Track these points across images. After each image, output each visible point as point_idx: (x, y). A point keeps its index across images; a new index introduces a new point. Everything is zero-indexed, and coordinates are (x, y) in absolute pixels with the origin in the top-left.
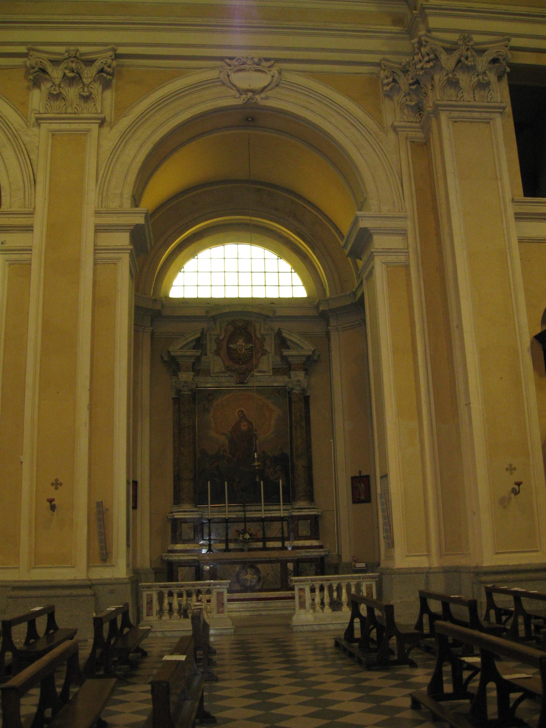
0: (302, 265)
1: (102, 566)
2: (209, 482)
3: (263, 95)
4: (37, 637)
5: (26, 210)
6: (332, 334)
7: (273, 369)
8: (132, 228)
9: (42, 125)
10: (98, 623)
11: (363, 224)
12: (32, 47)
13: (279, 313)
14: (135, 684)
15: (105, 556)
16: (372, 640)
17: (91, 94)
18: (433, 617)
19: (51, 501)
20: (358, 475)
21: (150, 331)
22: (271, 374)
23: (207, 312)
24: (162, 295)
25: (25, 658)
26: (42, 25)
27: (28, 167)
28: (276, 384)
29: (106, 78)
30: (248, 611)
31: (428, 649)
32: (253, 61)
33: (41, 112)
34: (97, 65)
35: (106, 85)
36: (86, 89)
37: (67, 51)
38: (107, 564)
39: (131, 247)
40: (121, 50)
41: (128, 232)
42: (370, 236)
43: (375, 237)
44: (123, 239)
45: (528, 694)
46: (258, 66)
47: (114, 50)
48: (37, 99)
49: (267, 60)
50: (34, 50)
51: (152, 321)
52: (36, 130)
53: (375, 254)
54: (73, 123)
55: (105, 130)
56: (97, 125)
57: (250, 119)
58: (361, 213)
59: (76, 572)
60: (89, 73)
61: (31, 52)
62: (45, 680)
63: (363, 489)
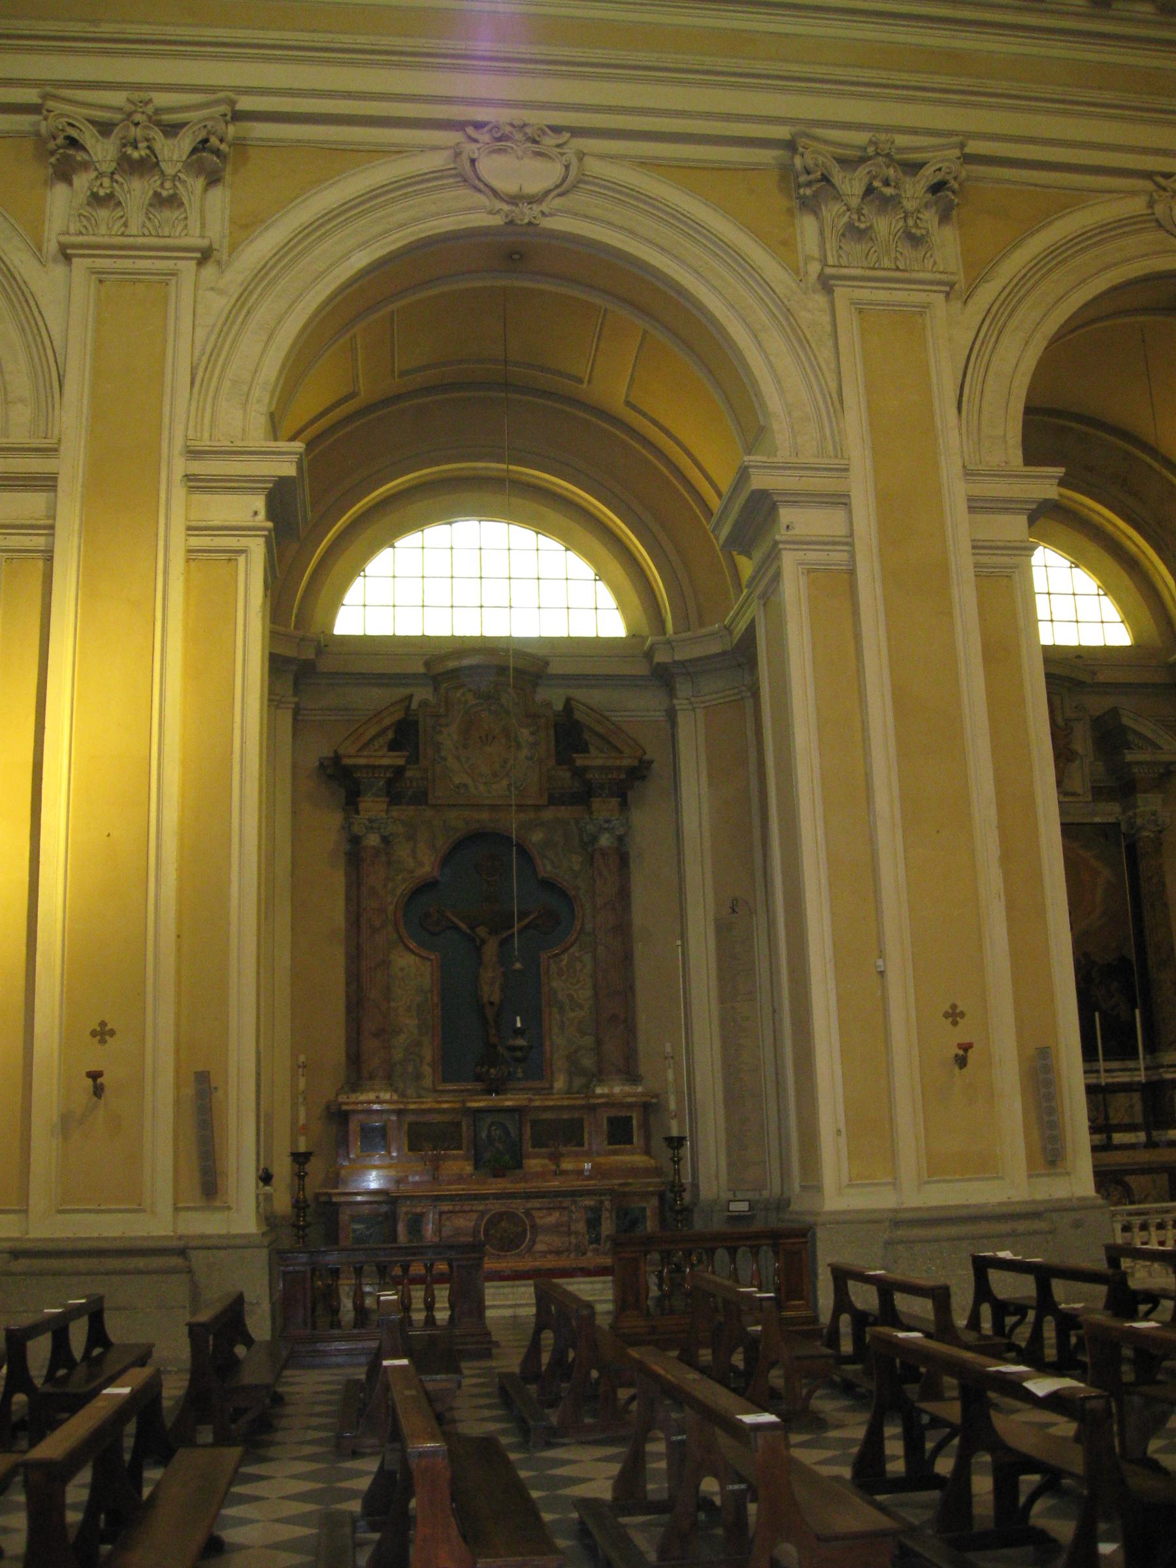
0: (1126, 580)
1: (1048, 1175)
2: (1097, 1014)
3: (544, 207)
4: (70, 1363)
5: (37, 442)
6: (681, 719)
7: (1093, 787)
9: (75, 260)
10: (195, 1331)
11: (759, 481)
12: (52, 88)
13: (554, 669)
14: (271, 1459)
15: (210, 1186)
16: (734, 1369)
17: (870, 228)
18: (861, 1320)
19: (94, 1076)
22: (1090, 799)
23: (427, 664)
25: (52, 1408)
26: (63, 44)
27: (45, 350)
28: (1097, 820)
29: (211, 160)
30: (314, 1310)
31: (847, 1388)
32: (526, 134)
34: (928, 176)
35: (214, 180)
36: (168, 185)
37: (871, 142)
38: (1058, 1170)
39: (270, 524)
40: (246, 103)
41: (1023, 514)
42: (774, 508)
44: (251, 508)
45: (1053, 1481)
46: (533, 140)
47: (233, 103)
48: (61, 205)
49: (556, 130)
50: (55, 97)
52: (59, 270)
53: (781, 546)
54: (895, 289)
55: (209, 271)
57: (516, 257)
58: (752, 458)
59: (157, 1223)
60: (173, 152)
61: (50, 104)
62: (100, 1448)
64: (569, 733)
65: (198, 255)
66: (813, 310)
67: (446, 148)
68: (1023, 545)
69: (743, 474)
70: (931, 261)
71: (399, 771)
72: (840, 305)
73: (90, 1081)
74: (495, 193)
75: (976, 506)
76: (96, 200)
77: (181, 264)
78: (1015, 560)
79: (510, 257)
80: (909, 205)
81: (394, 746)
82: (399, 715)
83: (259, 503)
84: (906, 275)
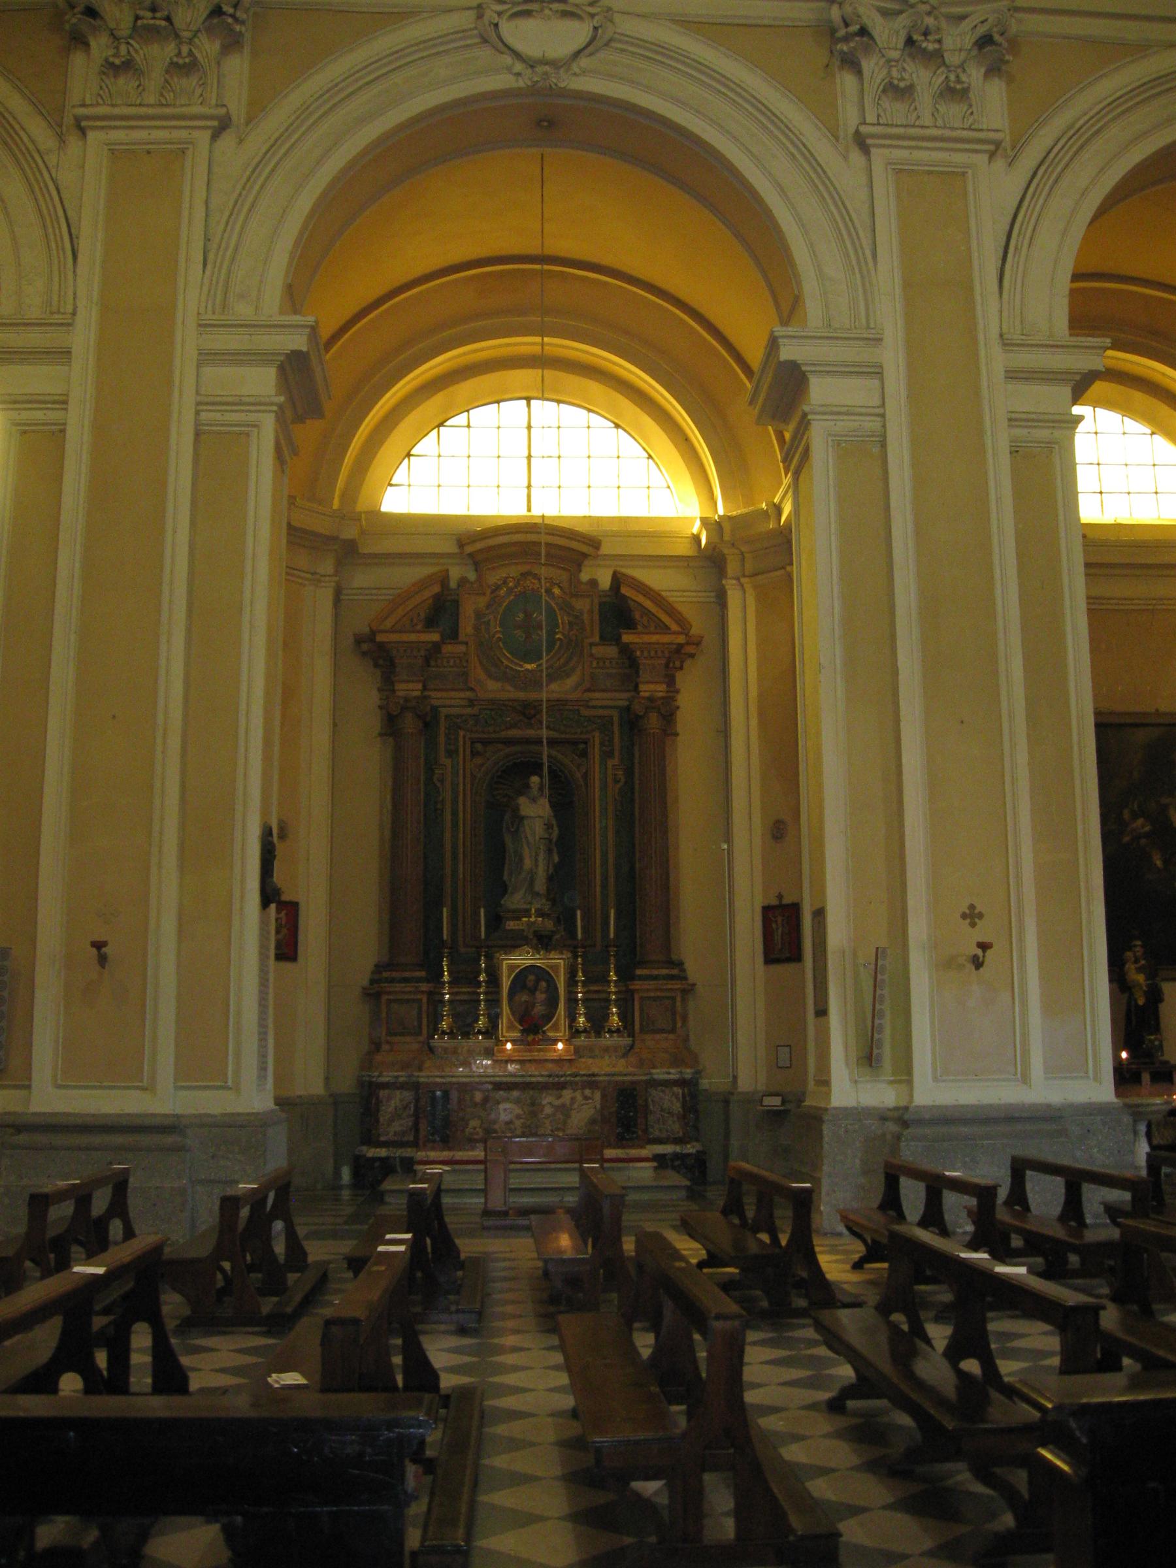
8: (282, 358)
11: (787, 353)
19: (98, 945)
20: (775, 902)
21: (333, 584)
24: (362, 506)
33: (88, 102)
35: (232, 44)
36: (123, 49)
43: (813, 381)
44: (262, 382)
51: (339, 564)
55: (227, 141)
56: (207, 134)
63: (786, 932)
64: (620, 610)
65: (216, 123)
66: (847, 172)
67: (469, 8)
68: (1062, 417)
69: (773, 344)
70: (915, 114)
71: (436, 647)
72: (878, 167)
73: (94, 950)
74: (517, 55)
75: (1013, 375)
76: (114, 69)
77: (196, 134)
78: (1057, 434)
79: (551, 124)
80: (952, 59)
81: (431, 622)
82: (436, 589)
83: (269, 375)
84: (167, 111)
